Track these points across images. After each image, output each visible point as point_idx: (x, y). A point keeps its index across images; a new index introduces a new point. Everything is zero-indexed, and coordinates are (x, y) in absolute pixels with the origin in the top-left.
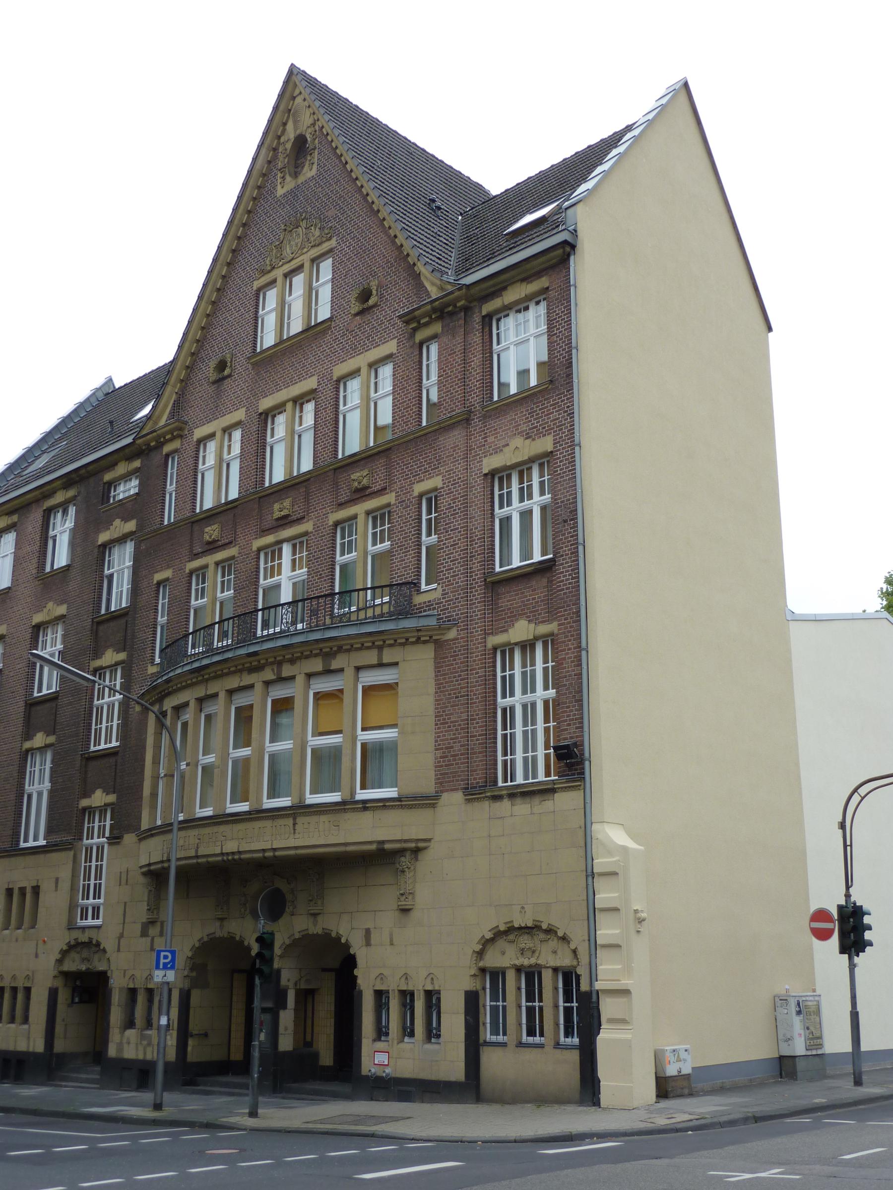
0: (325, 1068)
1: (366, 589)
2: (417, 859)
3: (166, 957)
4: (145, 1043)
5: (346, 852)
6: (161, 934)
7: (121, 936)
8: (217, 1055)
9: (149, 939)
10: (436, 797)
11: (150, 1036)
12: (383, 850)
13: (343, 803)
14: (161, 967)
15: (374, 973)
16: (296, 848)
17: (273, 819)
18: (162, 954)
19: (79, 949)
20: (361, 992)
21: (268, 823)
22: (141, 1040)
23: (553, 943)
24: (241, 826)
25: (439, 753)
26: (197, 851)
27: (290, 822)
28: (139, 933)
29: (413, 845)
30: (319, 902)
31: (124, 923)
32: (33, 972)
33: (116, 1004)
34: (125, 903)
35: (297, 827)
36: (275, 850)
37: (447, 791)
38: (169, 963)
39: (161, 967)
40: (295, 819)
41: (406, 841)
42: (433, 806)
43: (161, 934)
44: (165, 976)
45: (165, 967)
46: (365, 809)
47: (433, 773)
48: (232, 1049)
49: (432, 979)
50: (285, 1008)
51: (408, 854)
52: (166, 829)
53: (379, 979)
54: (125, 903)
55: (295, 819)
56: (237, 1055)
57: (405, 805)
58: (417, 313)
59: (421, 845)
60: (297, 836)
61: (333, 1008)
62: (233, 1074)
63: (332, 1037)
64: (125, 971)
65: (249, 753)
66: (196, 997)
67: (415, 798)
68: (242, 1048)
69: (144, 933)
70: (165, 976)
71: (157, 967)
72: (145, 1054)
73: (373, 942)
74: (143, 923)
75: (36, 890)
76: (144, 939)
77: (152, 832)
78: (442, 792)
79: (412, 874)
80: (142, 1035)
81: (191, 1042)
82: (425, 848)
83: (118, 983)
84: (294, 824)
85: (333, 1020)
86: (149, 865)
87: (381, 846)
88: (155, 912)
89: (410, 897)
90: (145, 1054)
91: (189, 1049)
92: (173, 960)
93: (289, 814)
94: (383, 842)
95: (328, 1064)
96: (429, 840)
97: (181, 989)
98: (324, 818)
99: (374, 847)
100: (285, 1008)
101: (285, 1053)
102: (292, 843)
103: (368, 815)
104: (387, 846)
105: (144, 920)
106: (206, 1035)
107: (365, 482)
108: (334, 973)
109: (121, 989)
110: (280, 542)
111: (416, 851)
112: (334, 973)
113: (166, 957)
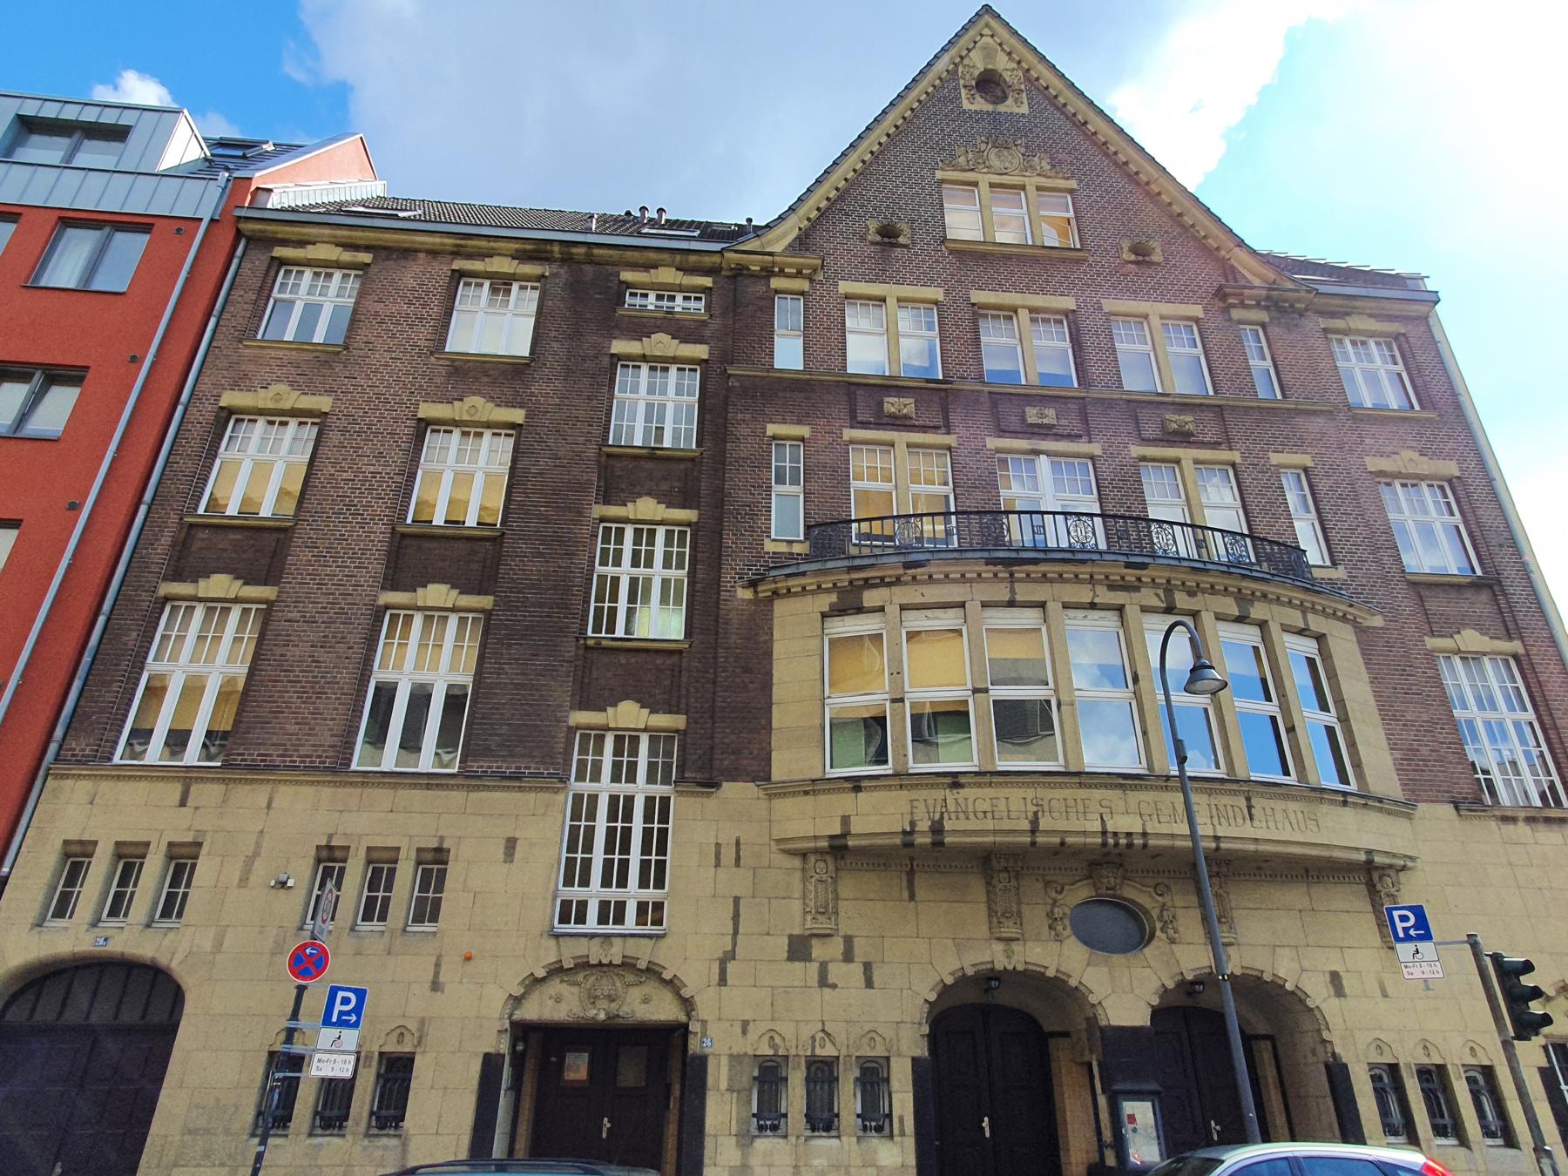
1: (947, 514)
3: (346, 1001)
5: (1172, 847)
6: (848, 957)
7: (731, 955)
9: (814, 967)
13: (896, 775)
18: (340, 994)
19: (580, 977)
23: (651, 988)
31: (736, 933)
32: (422, 1022)
33: (724, 1085)
34: (737, 900)
38: (348, 1013)
39: (334, 1019)
41: (1394, 856)
43: (848, 957)
45: (342, 1023)
53: (865, 1040)
54: (737, 900)
55: (1248, 799)
58: (1246, 292)
60: (1256, 823)
64: (745, 1024)
71: (327, 1021)
73: (1347, 990)
75: (182, 862)
83: (721, 1042)
84: (1249, 807)
92: (358, 1010)
102: (1247, 831)
107: (1190, 427)
109: (735, 1058)
110: (1037, 453)
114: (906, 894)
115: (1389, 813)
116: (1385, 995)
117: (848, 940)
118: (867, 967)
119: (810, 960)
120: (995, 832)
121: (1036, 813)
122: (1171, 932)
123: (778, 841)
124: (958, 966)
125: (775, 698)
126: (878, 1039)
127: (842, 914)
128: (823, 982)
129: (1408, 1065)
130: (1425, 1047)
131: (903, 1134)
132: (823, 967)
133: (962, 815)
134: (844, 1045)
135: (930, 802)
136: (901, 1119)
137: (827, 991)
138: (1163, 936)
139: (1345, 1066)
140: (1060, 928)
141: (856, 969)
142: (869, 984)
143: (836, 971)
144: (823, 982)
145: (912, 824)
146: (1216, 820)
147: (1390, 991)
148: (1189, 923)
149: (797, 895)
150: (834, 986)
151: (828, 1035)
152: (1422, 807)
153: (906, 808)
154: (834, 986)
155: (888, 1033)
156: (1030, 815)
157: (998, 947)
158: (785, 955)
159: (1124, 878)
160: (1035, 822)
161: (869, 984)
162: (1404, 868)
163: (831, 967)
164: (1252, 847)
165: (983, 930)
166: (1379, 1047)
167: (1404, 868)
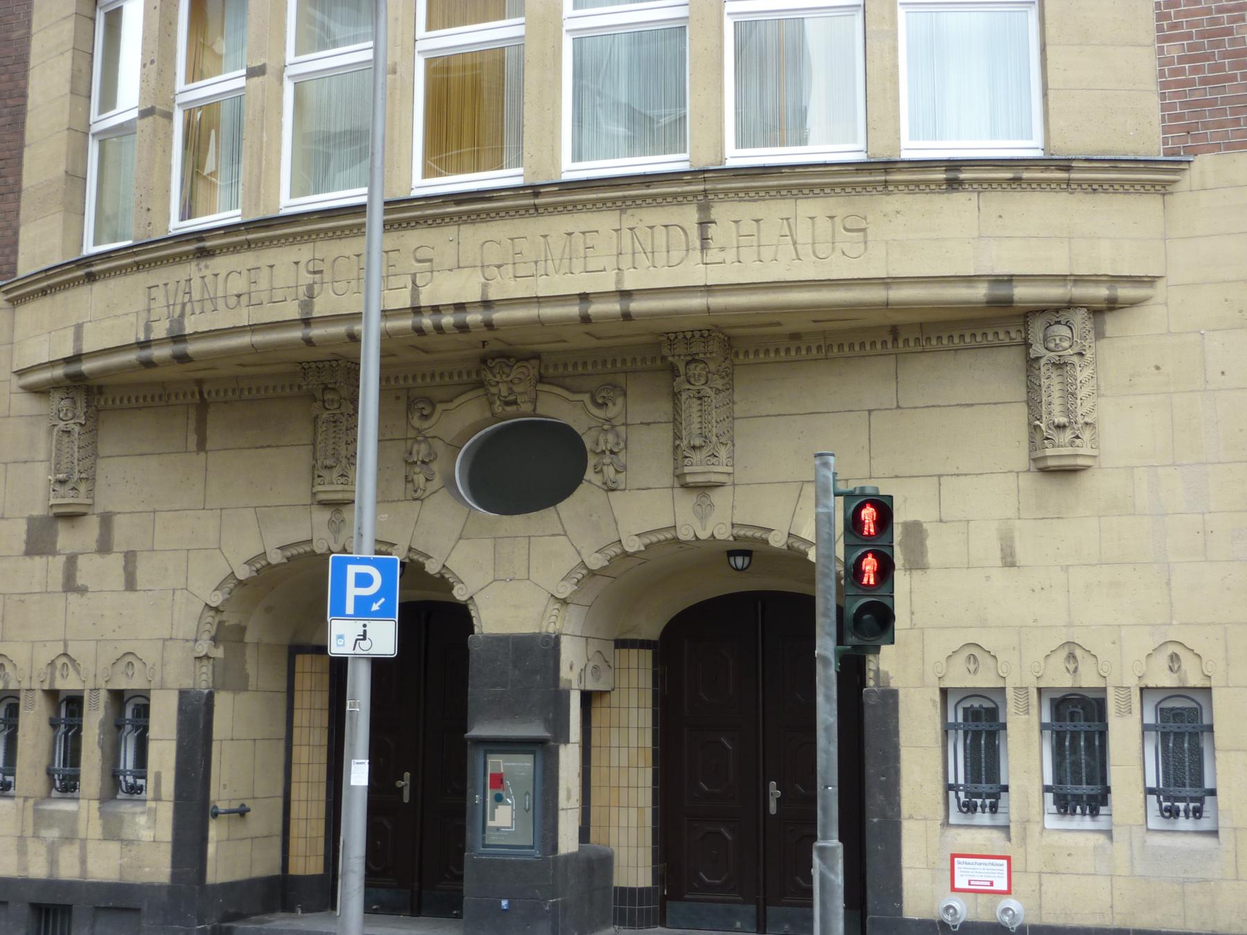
0: (628, 895)
2: (1100, 335)
4: (53, 834)
6: (104, 546)
8: (265, 864)
9: (58, 562)
10: (1174, 163)
11: (74, 817)
12: (1008, 302)
14: (350, 609)
15: (941, 644)
16: (708, 289)
17: (623, 211)
20: (890, 698)
21: (605, 222)
22: (36, 825)
24: (499, 231)
25: (1174, 50)
26: (308, 303)
27: (690, 216)
28: (21, 547)
29: (1103, 292)
30: (723, 453)
35: (712, 230)
36: (626, 295)
37: (1215, 148)
38: (374, 598)
39: (350, 609)
40: (704, 208)
41: (1079, 280)
42: (1163, 189)
43: (104, 546)
44: (364, 636)
46: (953, 184)
47: (1154, 103)
48: (296, 845)
49: (1174, 658)
50: (567, 741)
51: (1079, 318)
52: (87, 271)
53: (121, 666)
55: (704, 208)
56: (306, 863)
57: (1080, 183)
59: (1124, 292)
60: (713, 255)
61: (649, 742)
62: (305, 910)
63: (649, 813)
65: (520, 31)
66: (228, 716)
67: (1114, 163)
68: (321, 842)
69: (39, 541)
70: (364, 636)
72: (53, 862)
73: (932, 557)
74: (31, 520)
76: (38, 561)
77: (53, 281)
78: (1195, 151)
79: (1087, 372)
80: (37, 812)
81: (215, 831)
82: (1133, 303)
84: (703, 224)
85: (649, 772)
86: (77, 358)
87: (1001, 292)
88: (83, 488)
89: (1086, 435)
90: (53, 862)
91: (211, 849)
93: (685, 195)
94: (1010, 279)
95: (641, 885)
96: (1151, 281)
97: (183, 694)
98: (808, 207)
99: (980, 292)
100: (567, 741)
101: (569, 857)
102: (697, 274)
103: (961, 201)
104: (1021, 292)
105: (39, 510)
106: (242, 812)
108: (649, 653)
111: (1102, 311)
112: (649, 653)
113: (363, 580)
114: (193, 439)
115: (1094, 188)
116: (1009, 560)
117: (106, 520)
118: (130, 558)
119: (54, 553)
120: (254, 328)
121: (310, 288)
122: (610, 472)
123: (21, 373)
124: (256, 550)
125: (27, 142)
126: (137, 664)
127: (101, 481)
128: (70, 585)
129: (1022, 690)
130: (1072, 656)
131: (158, 798)
132: (72, 560)
133: (208, 306)
134: (89, 678)
135: (171, 287)
136: (158, 776)
137: (73, 597)
138: (597, 479)
139: (894, 694)
140: (420, 479)
141: (115, 562)
142: (130, 585)
143: (88, 568)
144: (70, 585)
145: (148, 329)
146: (626, 261)
147: (1021, 556)
148: (648, 453)
149: (42, 456)
150: (83, 590)
151: (73, 661)
152: (1204, 166)
153: (140, 303)
154: (83, 590)
155: (150, 654)
156: (302, 290)
157: (686, 503)
158: (23, 547)
159: (541, 379)
160: (308, 303)
161: (130, 585)
162: (1112, 305)
163: (82, 562)
164: (696, 302)
165: (301, 493)
166: (972, 658)
167: (1112, 305)
